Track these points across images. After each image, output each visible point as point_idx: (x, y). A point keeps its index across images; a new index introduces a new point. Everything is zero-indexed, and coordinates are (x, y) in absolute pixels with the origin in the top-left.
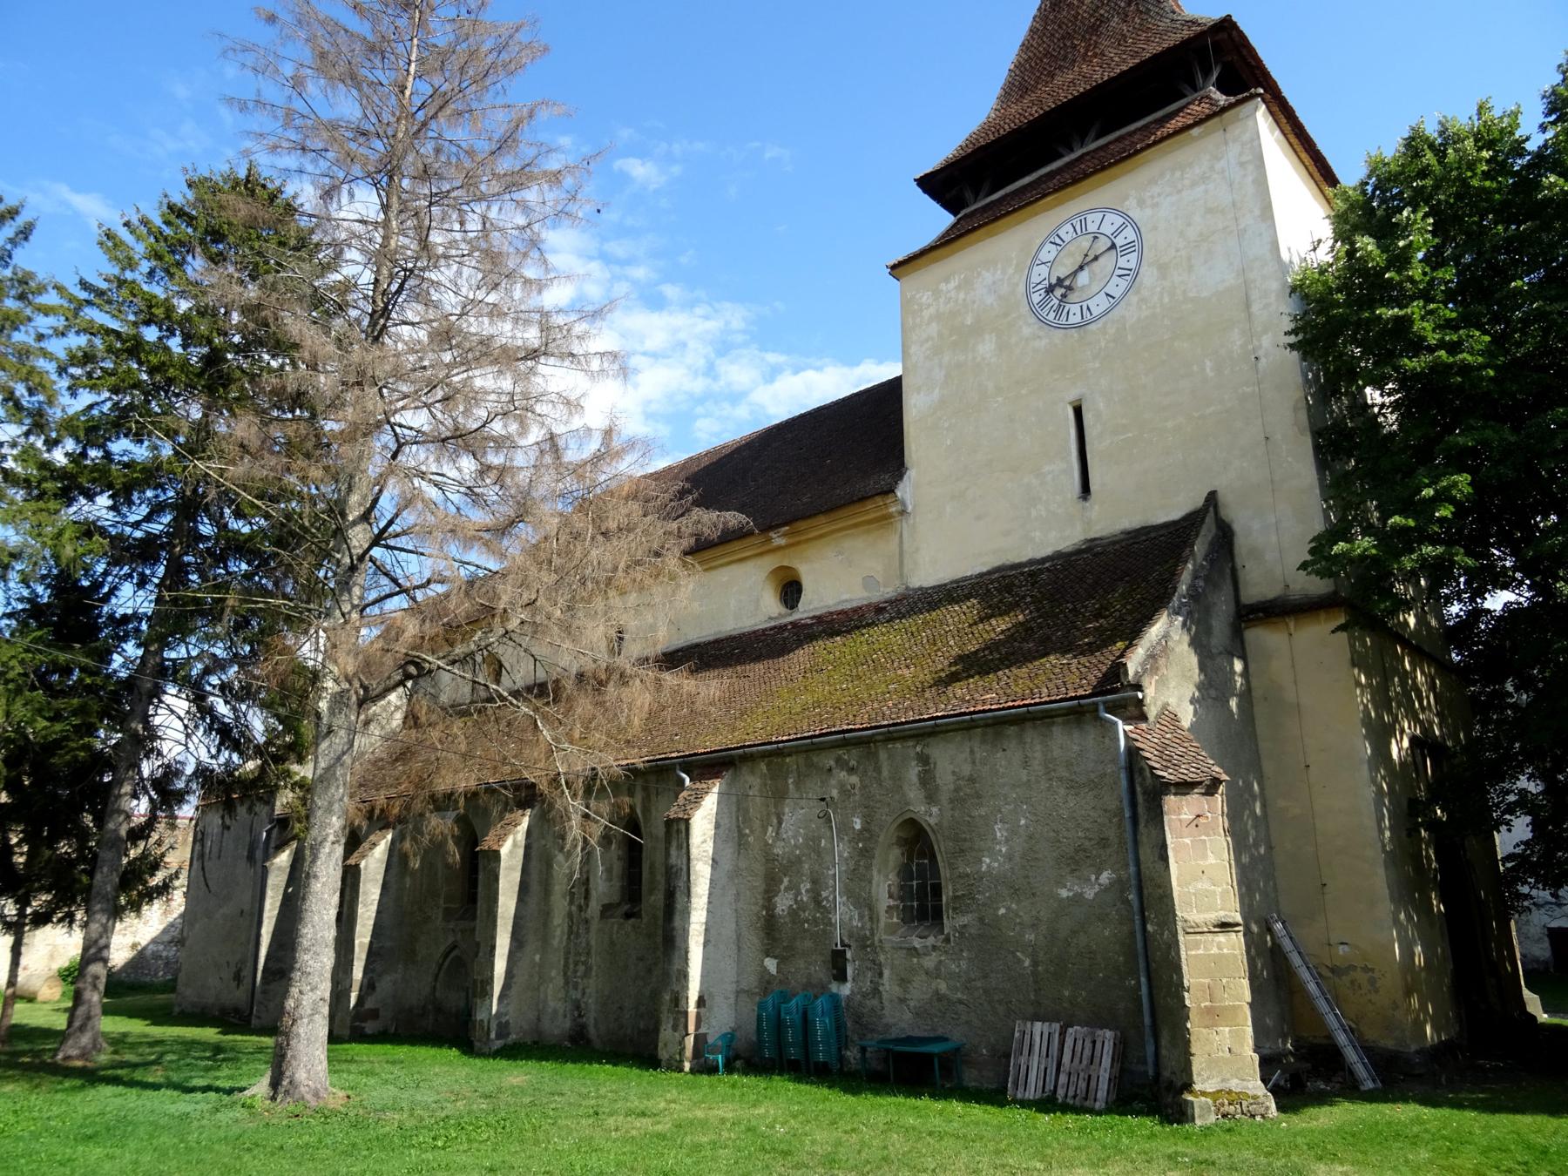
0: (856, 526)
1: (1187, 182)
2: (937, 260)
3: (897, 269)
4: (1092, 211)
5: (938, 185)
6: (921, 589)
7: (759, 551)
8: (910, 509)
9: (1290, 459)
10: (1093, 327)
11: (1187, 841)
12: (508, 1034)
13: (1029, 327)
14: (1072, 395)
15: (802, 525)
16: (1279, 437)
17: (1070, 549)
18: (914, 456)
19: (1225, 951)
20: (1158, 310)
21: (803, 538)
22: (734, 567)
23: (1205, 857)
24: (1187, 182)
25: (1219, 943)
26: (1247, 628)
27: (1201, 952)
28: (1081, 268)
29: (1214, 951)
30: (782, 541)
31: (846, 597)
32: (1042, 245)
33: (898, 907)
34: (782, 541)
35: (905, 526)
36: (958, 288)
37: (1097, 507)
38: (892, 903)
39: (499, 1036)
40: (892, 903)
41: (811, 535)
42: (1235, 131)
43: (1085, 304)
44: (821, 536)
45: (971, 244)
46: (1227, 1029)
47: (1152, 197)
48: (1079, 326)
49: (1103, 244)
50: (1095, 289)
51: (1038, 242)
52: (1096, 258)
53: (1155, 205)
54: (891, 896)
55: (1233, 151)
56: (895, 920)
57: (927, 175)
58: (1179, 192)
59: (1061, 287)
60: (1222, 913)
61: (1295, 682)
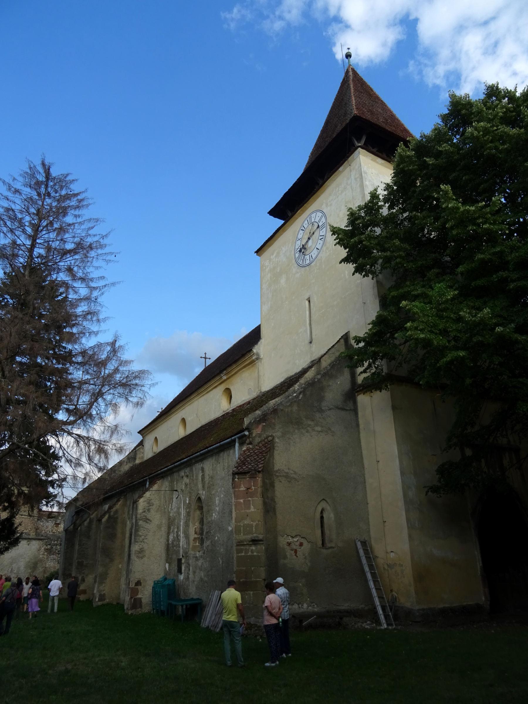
0: (245, 367)
1: (340, 192)
2: (270, 246)
3: (259, 251)
4: (313, 213)
5: (275, 212)
6: (265, 391)
7: (219, 383)
8: (262, 356)
9: (372, 312)
10: (312, 264)
11: (242, 501)
12: (105, 600)
13: (295, 269)
14: (307, 297)
15: (229, 369)
16: (368, 302)
17: (306, 367)
18: (263, 333)
19: (255, 554)
20: (331, 252)
21: (230, 375)
22: (214, 390)
23: (249, 508)
24: (340, 192)
25: (252, 550)
26: (358, 395)
27: (243, 554)
28: (309, 239)
29: (250, 554)
30: (225, 378)
31: (243, 399)
32: (299, 231)
33: (199, 538)
34: (225, 378)
35: (259, 364)
36: (276, 257)
37: (314, 346)
38: (196, 536)
39: (99, 600)
40: (196, 536)
41: (232, 374)
42: (353, 164)
43: (310, 254)
44: (236, 373)
45: (279, 237)
46: (252, 593)
47: (330, 201)
48: (309, 265)
49: (316, 225)
50: (313, 247)
51: (298, 230)
52: (313, 233)
53: (331, 205)
54: (196, 533)
55: (353, 173)
56: (197, 544)
57: (271, 210)
58: (338, 197)
59: (303, 249)
60: (255, 535)
61: (373, 420)
